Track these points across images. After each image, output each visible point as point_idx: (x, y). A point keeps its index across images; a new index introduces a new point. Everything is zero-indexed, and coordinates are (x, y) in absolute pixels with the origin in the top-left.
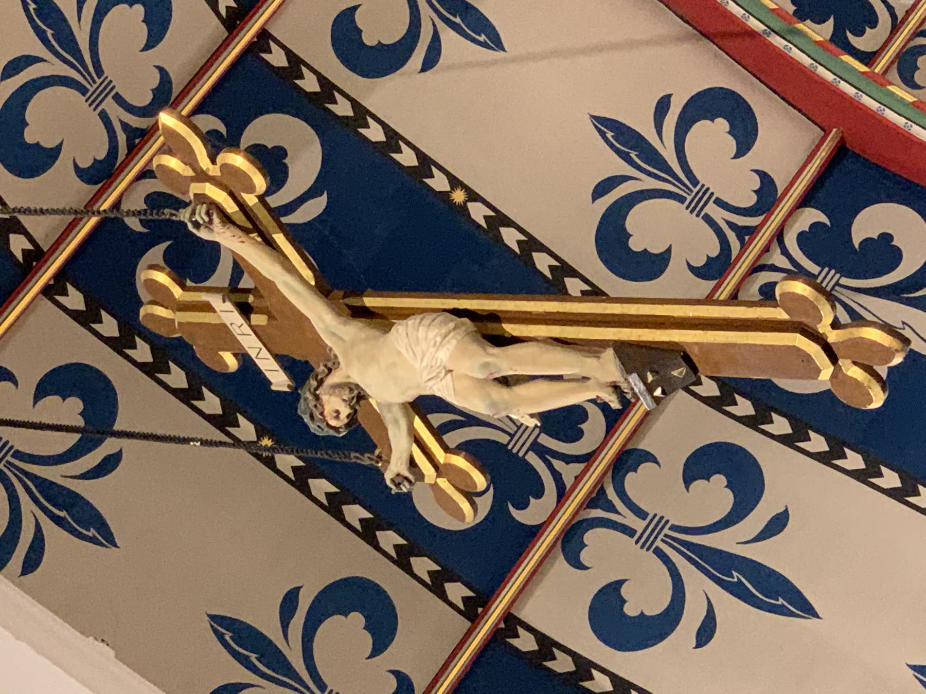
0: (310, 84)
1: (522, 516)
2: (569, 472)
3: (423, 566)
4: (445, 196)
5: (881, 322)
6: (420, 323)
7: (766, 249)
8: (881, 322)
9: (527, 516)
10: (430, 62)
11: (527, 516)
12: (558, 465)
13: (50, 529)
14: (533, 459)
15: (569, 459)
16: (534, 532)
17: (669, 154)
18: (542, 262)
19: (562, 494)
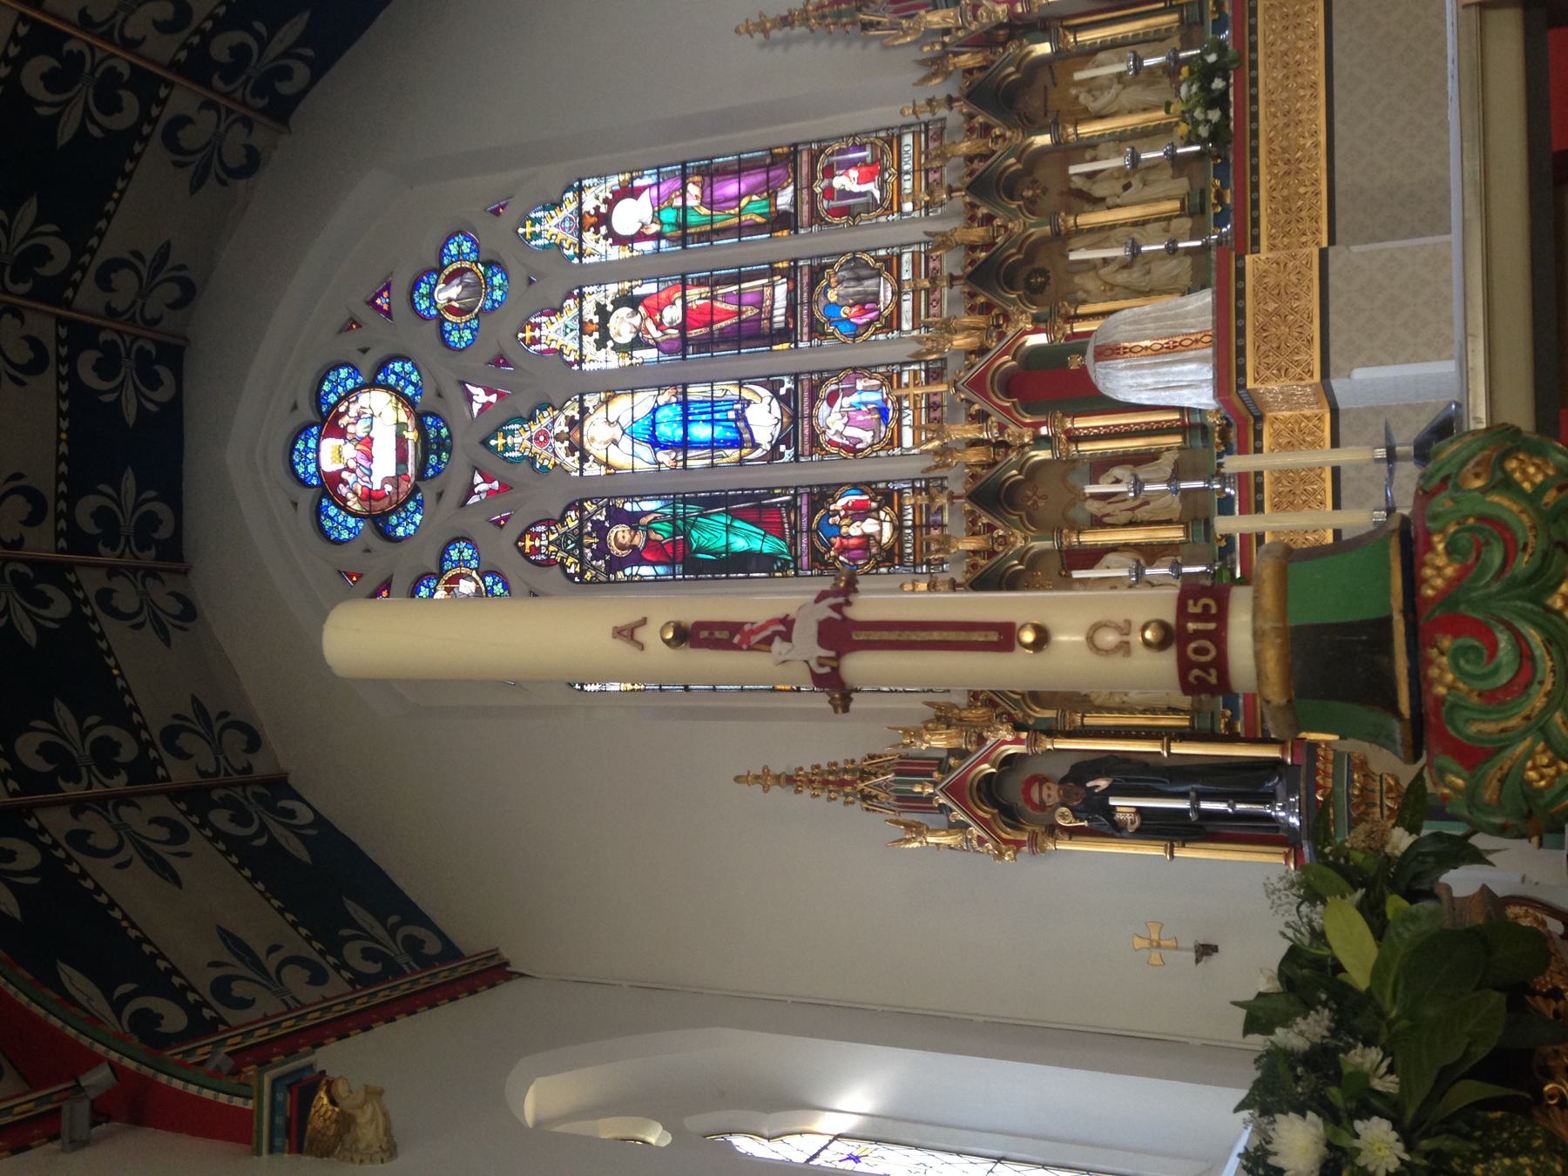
0: (63, 524)
1: (101, 548)
2: (99, 56)
3: (155, 111)
4: (67, 442)
5: (1082, 310)
6: (1275, 1154)
7: (129, 334)
8: (1082, 310)
9: (126, 71)
10: (176, 164)
11: (126, 71)
12: (127, 550)
13: (192, 168)
14: (123, 540)
15: (93, 56)
16: (133, 66)
17: (160, 277)
18: (64, 388)
19: (112, 56)
